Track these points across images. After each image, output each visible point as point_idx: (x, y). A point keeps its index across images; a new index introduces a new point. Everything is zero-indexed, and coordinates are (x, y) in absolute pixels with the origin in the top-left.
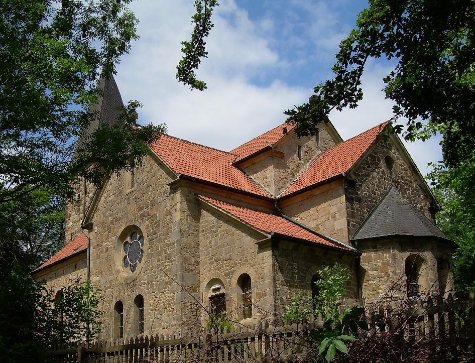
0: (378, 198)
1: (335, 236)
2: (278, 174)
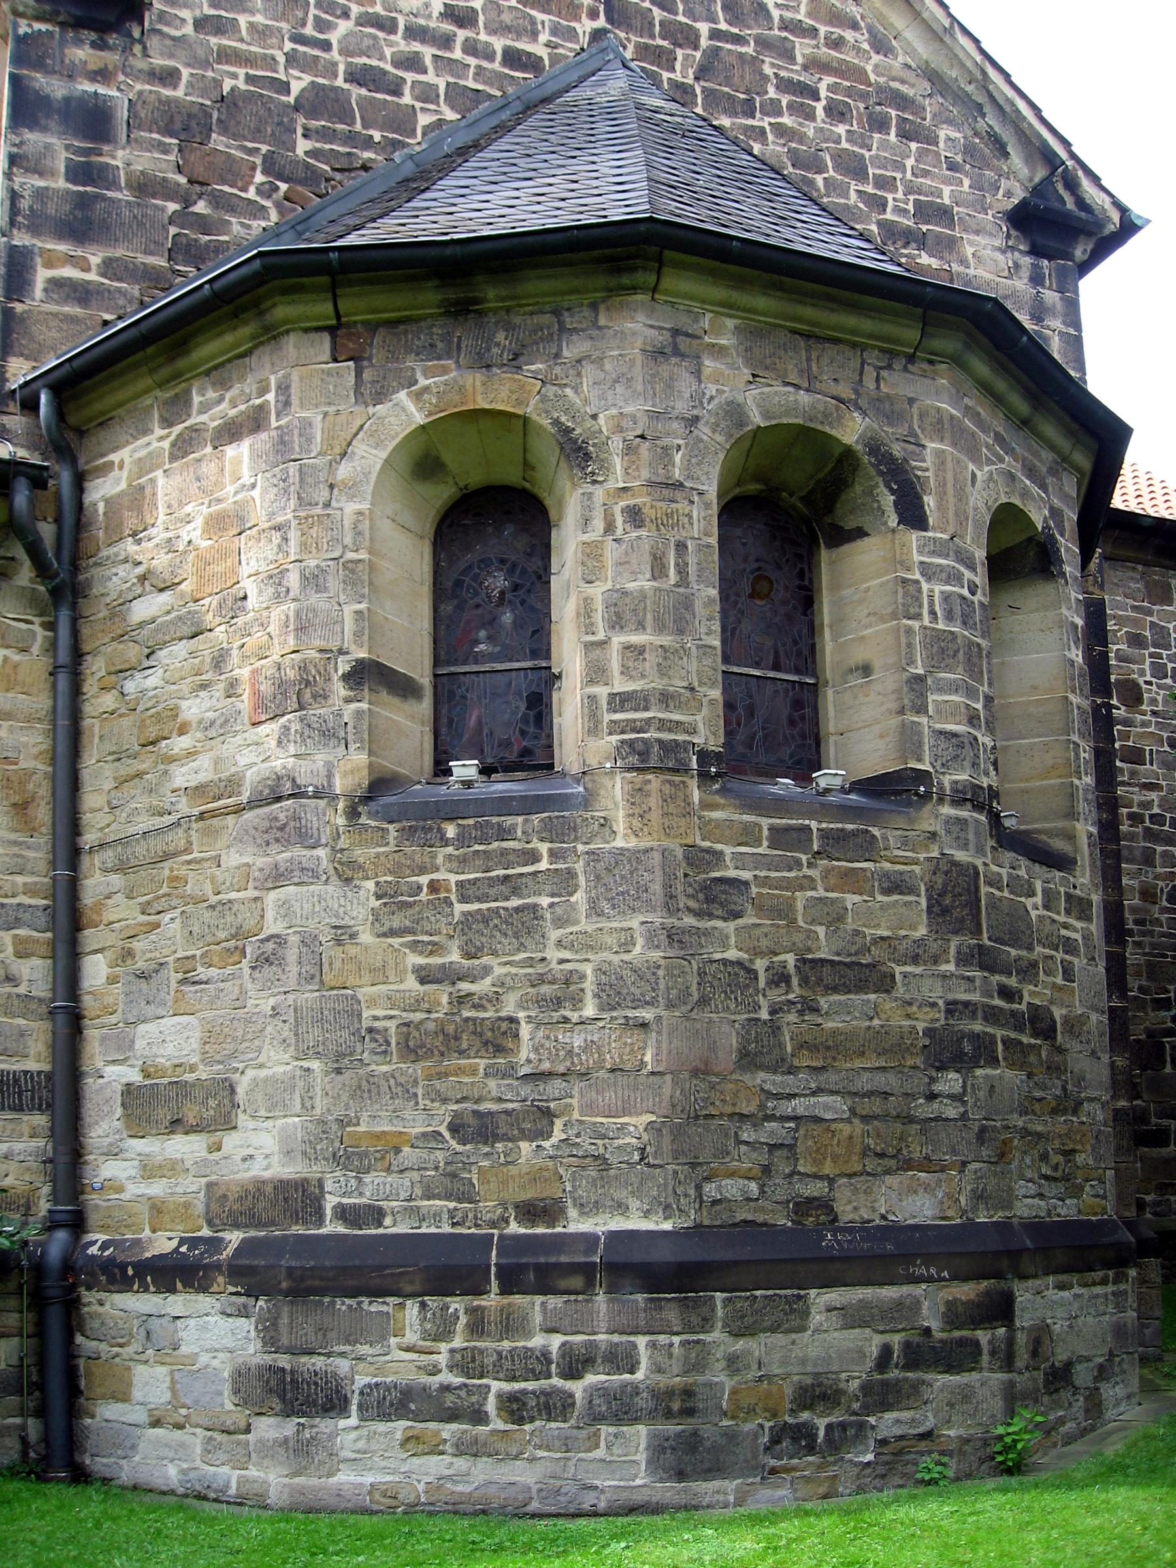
0: (424, 120)
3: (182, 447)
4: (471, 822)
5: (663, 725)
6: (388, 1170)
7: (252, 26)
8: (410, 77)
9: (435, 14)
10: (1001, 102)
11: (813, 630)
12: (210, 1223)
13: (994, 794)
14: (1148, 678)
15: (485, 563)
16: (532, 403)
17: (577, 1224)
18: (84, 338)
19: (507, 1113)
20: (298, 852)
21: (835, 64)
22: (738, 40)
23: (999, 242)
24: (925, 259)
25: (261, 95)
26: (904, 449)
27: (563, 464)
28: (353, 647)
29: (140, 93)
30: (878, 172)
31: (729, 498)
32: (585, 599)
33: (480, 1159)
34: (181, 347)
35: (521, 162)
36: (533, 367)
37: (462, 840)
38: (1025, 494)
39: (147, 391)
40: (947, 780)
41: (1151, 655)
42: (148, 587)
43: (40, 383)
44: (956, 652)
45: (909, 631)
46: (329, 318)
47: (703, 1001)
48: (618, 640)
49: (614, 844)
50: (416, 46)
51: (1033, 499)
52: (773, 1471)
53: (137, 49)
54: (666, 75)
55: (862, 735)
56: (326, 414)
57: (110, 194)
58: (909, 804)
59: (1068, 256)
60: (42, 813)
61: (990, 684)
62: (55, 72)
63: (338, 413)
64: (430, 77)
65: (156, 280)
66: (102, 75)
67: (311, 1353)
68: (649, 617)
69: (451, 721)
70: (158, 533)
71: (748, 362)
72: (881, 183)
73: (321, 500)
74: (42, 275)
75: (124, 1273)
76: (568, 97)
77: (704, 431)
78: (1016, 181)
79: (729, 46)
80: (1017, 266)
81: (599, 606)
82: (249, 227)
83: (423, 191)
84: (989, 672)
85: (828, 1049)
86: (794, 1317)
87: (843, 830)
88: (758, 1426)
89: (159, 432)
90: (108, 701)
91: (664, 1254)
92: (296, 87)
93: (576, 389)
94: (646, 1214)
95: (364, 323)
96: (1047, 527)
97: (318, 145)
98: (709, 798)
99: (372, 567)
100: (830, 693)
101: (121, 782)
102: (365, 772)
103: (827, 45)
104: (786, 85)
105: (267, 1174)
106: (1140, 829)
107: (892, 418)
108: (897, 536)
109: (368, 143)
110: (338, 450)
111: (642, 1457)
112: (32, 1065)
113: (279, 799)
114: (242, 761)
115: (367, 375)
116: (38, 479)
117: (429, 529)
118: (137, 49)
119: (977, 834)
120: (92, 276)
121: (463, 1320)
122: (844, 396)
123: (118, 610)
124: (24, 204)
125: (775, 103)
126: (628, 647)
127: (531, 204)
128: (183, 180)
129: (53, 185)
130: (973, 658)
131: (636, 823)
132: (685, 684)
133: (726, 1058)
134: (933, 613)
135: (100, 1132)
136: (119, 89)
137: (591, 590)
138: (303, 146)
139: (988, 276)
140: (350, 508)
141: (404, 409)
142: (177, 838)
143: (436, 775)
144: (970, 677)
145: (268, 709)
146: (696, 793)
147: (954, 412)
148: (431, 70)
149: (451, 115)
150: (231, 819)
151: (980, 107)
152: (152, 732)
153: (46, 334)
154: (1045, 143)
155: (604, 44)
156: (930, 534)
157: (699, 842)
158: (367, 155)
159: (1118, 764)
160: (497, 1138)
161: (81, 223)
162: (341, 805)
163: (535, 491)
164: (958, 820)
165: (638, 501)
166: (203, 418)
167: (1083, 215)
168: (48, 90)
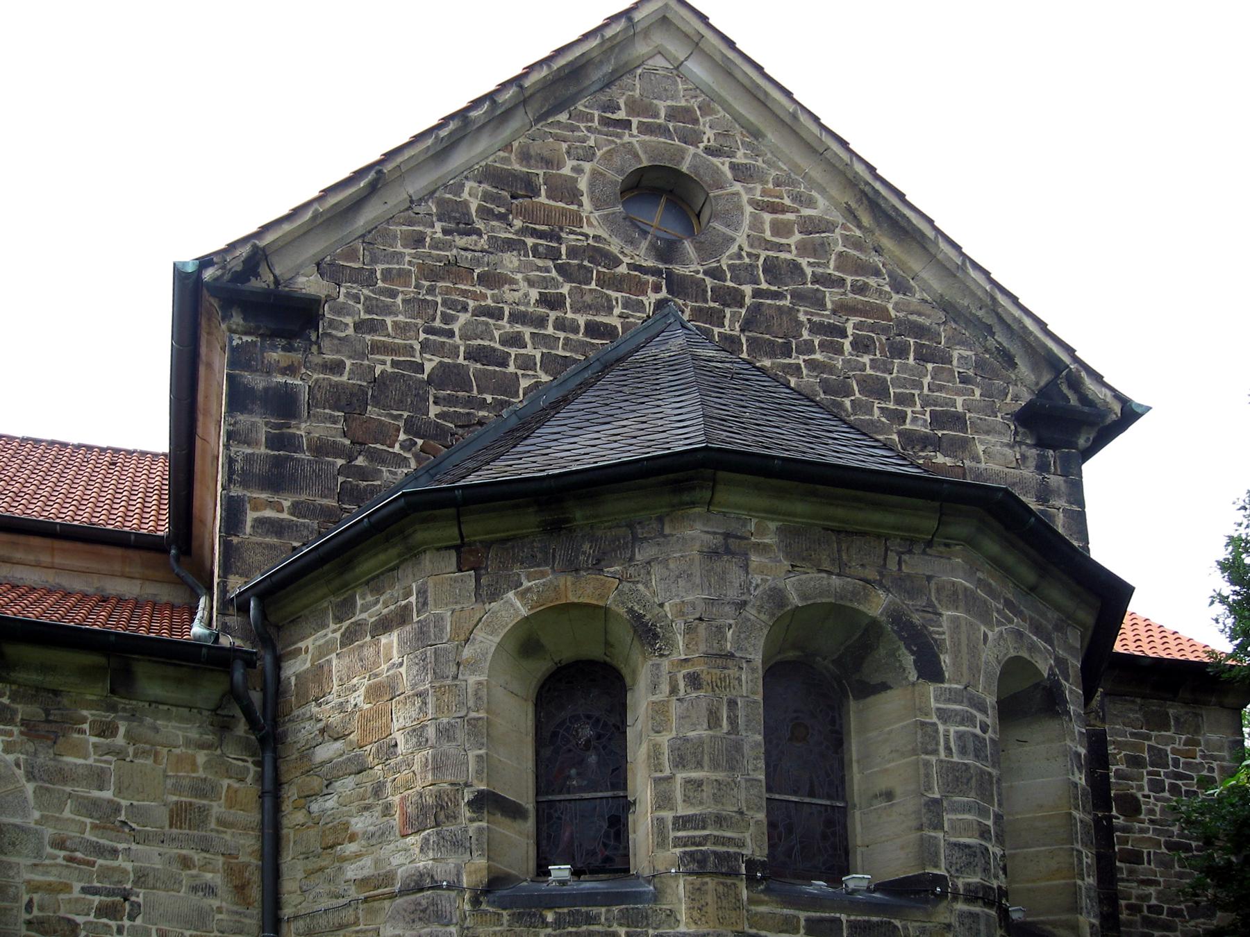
0: (524, 383)
3: (349, 637)
4: (566, 910)
5: (718, 840)
7: (395, 324)
8: (513, 351)
9: (533, 301)
10: (1009, 322)
11: (842, 765)
13: (1003, 893)
14: (1146, 792)
15: (576, 718)
16: (612, 596)
18: (279, 559)
21: (860, 306)
22: (777, 295)
24: (940, 459)
25: (403, 375)
26: (924, 618)
27: (636, 642)
28: (475, 782)
29: (317, 380)
30: (898, 391)
31: (772, 663)
32: (654, 746)
34: (347, 565)
35: (599, 410)
36: (612, 569)
37: (558, 923)
38: (1032, 648)
39: (324, 597)
40: (960, 883)
41: (1149, 773)
43: (250, 593)
44: (969, 780)
45: (927, 764)
46: (454, 539)
48: (680, 776)
49: (678, 930)
50: (518, 328)
51: (1039, 651)
53: (314, 348)
54: (716, 330)
55: (885, 845)
56: (453, 611)
57: (296, 455)
58: (927, 901)
59: (1074, 446)
60: (255, 893)
61: (1000, 805)
62: (257, 371)
63: (462, 610)
64: (529, 350)
65: (330, 516)
66: (290, 370)
68: (706, 758)
69: (549, 836)
70: (333, 699)
71: (788, 555)
72: (900, 399)
73: (451, 674)
74: (251, 516)
76: (638, 356)
77: (751, 612)
78: (1023, 385)
79: (769, 302)
80: (1024, 457)
81: (666, 751)
82: (395, 473)
83: (525, 439)
84: (999, 794)
87: (868, 921)
89: (333, 626)
90: (300, 817)
92: (428, 367)
95: (481, 542)
96: (1052, 673)
97: (445, 409)
98: (755, 896)
99: (489, 723)
100: (857, 814)
101: (309, 874)
102: (485, 872)
103: (853, 291)
104: (816, 328)
106: (1138, 918)
107: (912, 593)
108: (917, 688)
109: (483, 404)
110: (462, 637)
113: (421, 890)
114: (396, 861)
116: (249, 661)
117: (532, 693)
118: (314, 348)
119: (988, 925)
120: (285, 516)
122: (870, 578)
123: (306, 754)
124: (238, 466)
126: (688, 781)
127: (610, 442)
128: (348, 442)
129: (257, 451)
130: (985, 785)
131: (696, 914)
132: (736, 809)
134: (948, 748)
136: (302, 379)
138: (434, 410)
139: (997, 468)
140: (472, 680)
141: (512, 605)
142: (349, 915)
143: (538, 875)
144: (982, 800)
145: (413, 825)
146: (745, 892)
147: (967, 584)
148: (529, 345)
149: (545, 378)
150: (387, 903)
152: (330, 840)
153: (254, 558)
154: (1050, 351)
155: (666, 311)
156: (946, 685)
157: (747, 929)
158: (481, 413)
159: (1118, 864)
161: (277, 477)
162: (467, 896)
163: (614, 663)
164: (971, 914)
165: (698, 669)
166: (364, 616)
167: (1086, 409)
168: (253, 384)
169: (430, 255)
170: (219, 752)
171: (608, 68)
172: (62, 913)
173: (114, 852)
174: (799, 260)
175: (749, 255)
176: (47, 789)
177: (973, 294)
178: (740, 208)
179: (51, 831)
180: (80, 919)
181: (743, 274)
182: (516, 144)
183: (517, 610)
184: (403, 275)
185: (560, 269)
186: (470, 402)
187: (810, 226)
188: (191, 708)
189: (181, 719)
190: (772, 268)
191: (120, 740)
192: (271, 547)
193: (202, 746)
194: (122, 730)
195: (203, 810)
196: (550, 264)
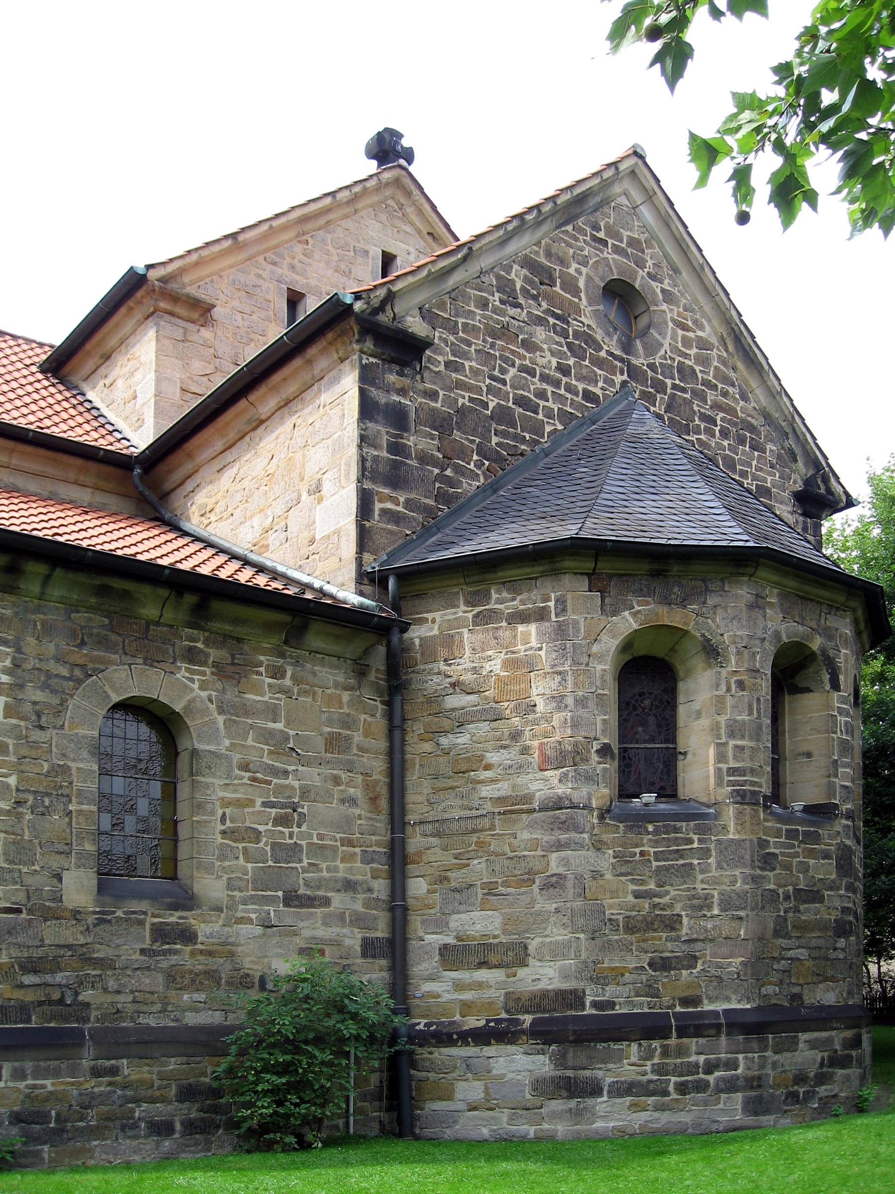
0: (548, 429)
1: (314, 560)
2: (177, 375)
6: (618, 984)
8: (542, 403)
12: (507, 1011)
17: (708, 1007)
19: (676, 957)
20: (573, 835)
22: (684, 390)
23: (790, 509)
29: (421, 403)
33: (663, 978)
37: (656, 832)
42: (458, 691)
47: (763, 908)
48: (732, 743)
50: (545, 386)
52: (786, 1111)
53: (418, 377)
58: (831, 819)
60: (384, 803)
64: (550, 404)
66: (402, 392)
67: (584, 1069)
74: (378, 506)
75: (446, 1036)
77: (767, 644)
78: (799, 474)
81: (723, 726)
82: (471, 485)
85: (803, 927)
86: (793, 1046)
88: (781, 1092)
90: (428, 747)
91: (750, 1019)
92: (491, 405)
93: (714, 620)
94: (739, 1002)
101: (437, 791)
105: (550, 987)
109: (523, 440)
110: (593, 638)
111: (739, 1107)
112: (380, 934)
113: (561, 809)
114: (534, 787)
115: (607, 600)
120: (400, 509)
121: (659, 1050)
124: (368, 464)
125: (698, 426)
126: (736, 747)
131: (739, 828)
133: (769, 933)
135: (420, 968)
137: (719, 718)
138: (495, 440)
140: (599, 667)
149: (560, 427)
150: (524, 816)
151: (787, 434)
153: (380, 540)
158: (523, 447)
160: (671, 969)
169: (492, 318)
170: (358, 693)
171: (598, 199)
172: (248, 824)
173: (286, 773)
174: (695, 367)
175: (671, 358)
176: (234, 721)
177: (782, 411)
178: (666, 323)
179: (239, 756)
180: (261, 828)
181: (667, 371)
182: (543, 242)
183: (630, 624)
184: (475, 329)
185: (569, 345)
186: (516, 437)
187: (703, 344)
188: (339, 658)
189: (332, 666)
190: (681, 368)
191: (287, 682)
192: (390, 532)
193: (346, 688)
194: (289, 673)
195: (348, 739)
196: (563, 340)
